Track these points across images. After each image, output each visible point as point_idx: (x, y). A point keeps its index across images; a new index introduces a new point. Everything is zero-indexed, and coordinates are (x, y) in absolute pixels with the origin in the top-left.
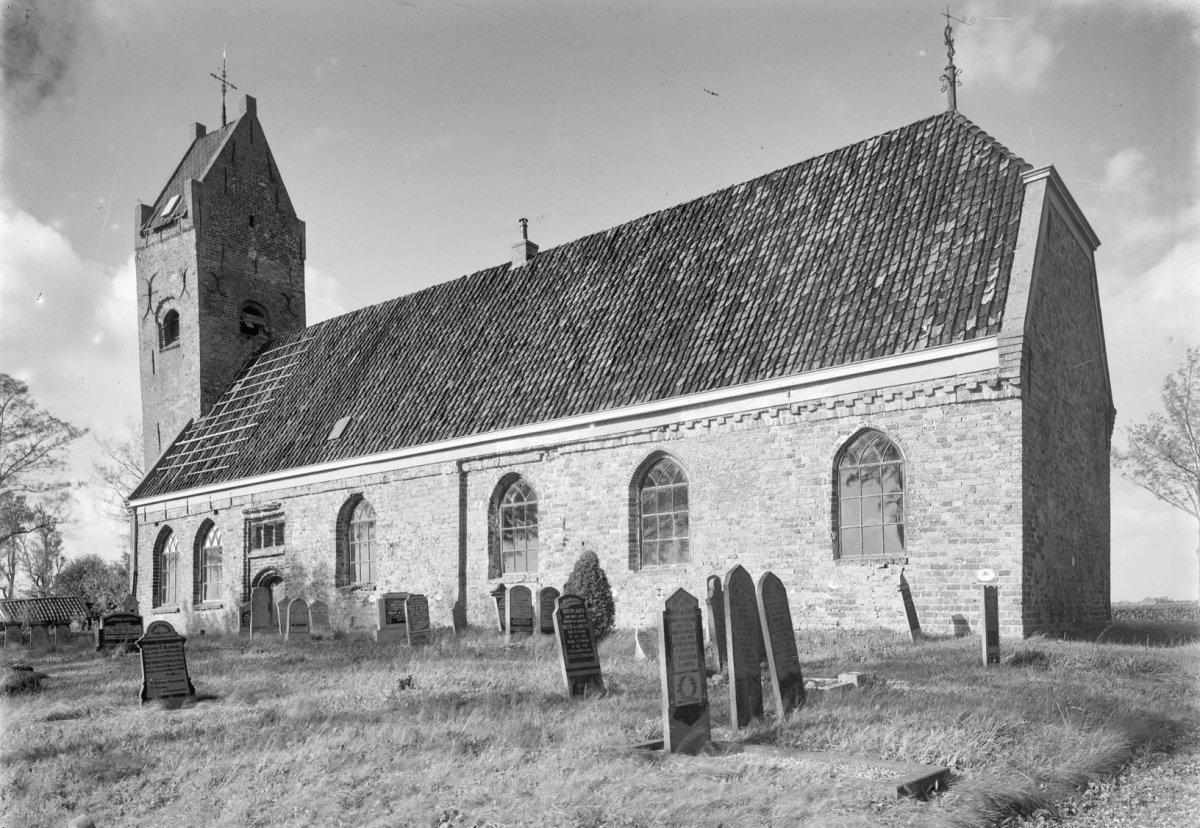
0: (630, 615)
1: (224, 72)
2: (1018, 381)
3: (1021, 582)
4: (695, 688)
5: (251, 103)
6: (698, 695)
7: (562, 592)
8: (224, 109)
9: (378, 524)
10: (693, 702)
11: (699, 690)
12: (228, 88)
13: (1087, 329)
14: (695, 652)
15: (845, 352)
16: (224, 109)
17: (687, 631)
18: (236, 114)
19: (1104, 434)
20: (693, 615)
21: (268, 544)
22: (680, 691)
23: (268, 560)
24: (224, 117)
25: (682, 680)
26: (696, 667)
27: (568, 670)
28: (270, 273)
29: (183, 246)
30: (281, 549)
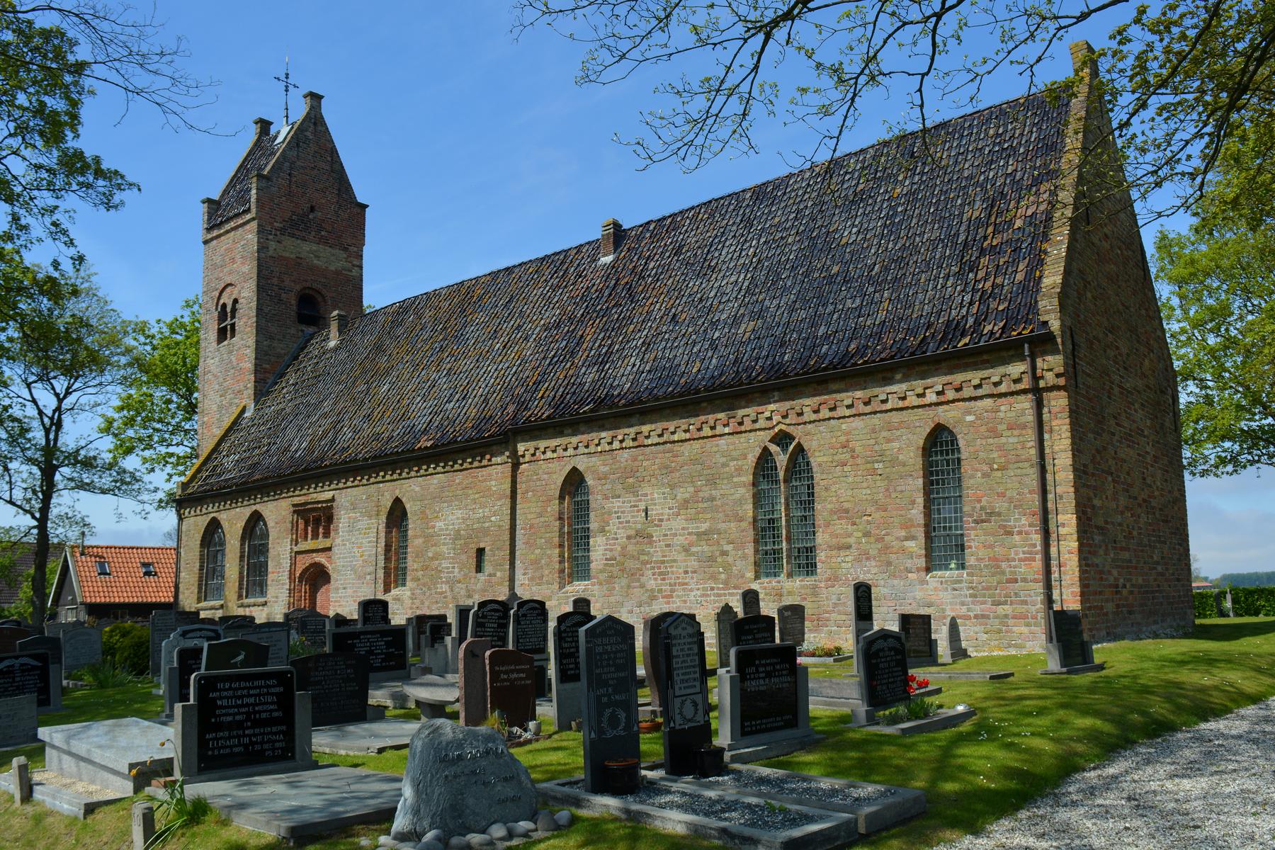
2: (660, 759)
3: (1077, 574)
4: (697, 710)
6: (700, 718)
11: (701, 712)
12: (291, 88)
13: (1143, 312)
14: (698, 675)
15: (1197, 41)
17: (688, 655)
18: (300, 111)
19: (753, 800)
22: (681, 713)
25: (683, 703)
26: (698, 690)
28: (326, 258)
29: (244, 240)
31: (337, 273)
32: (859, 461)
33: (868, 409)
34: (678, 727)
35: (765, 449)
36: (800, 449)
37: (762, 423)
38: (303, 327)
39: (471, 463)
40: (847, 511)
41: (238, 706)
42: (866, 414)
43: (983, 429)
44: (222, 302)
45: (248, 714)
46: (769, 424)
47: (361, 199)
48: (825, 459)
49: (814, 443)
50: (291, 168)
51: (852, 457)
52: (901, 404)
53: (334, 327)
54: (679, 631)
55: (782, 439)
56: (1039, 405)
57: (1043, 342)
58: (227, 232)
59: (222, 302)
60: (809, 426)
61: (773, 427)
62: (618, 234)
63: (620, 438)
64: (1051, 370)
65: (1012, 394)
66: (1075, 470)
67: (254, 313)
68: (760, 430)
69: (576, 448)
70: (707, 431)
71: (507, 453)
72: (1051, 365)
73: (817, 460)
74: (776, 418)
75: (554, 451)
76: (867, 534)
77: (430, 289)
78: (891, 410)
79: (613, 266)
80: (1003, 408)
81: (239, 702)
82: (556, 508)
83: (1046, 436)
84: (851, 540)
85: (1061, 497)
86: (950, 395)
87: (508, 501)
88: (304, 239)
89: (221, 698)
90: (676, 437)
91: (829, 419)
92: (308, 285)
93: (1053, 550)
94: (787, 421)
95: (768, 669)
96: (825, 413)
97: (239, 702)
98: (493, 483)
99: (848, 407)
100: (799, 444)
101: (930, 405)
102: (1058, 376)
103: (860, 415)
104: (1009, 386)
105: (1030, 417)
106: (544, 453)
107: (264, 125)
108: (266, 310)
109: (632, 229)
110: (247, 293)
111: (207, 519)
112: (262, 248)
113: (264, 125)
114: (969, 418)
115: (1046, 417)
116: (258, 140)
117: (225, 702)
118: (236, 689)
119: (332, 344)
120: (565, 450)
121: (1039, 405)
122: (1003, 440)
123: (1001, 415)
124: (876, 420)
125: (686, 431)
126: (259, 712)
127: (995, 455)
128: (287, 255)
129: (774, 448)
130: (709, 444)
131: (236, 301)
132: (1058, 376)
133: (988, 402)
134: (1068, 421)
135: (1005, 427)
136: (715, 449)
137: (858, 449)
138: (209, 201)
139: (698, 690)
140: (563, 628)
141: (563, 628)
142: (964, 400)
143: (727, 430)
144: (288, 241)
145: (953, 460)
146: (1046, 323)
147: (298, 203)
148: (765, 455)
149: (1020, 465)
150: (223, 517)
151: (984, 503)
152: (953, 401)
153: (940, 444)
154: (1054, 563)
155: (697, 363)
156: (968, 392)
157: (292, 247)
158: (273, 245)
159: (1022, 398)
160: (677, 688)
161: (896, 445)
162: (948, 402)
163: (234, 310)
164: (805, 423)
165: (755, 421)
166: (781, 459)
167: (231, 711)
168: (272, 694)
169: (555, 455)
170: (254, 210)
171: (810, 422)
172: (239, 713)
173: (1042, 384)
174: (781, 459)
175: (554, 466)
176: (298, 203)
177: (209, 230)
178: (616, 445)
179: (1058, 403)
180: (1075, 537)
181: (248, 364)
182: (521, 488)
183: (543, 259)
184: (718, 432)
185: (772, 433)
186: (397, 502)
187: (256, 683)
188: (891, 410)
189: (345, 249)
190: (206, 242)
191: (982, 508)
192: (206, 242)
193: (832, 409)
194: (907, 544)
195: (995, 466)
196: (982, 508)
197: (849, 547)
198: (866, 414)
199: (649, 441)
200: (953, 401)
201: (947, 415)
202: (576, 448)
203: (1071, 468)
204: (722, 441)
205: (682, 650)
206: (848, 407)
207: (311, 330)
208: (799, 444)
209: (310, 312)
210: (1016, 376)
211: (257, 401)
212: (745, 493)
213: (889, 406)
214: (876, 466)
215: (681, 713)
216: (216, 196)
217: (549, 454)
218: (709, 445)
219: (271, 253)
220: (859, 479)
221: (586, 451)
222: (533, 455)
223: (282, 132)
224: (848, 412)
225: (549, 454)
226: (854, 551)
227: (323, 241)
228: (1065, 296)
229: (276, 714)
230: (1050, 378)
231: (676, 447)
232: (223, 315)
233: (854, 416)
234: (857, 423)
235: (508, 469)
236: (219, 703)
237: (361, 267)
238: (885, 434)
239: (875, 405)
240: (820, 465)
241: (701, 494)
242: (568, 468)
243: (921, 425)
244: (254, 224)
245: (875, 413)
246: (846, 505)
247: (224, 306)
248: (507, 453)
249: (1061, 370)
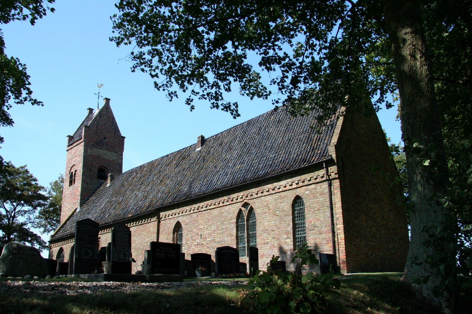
18: (102, 104)
26: (127, 250)
28: (109, 155)
29: (80, 149)
31: (113, 161)
32: (271, 211)
33: (274, 192)
34: (116, 261)
36: (252, 209)
37: (239, 200)
38: (100, 180)
39: (144, 222)
40: (267, 230)
42: (273, 194)
43: (312, 196)
44: (71, 171)
46: (242, 200)
47: (123, 135)
48: (260, 211)
49: (256, 206)
50: (97, 124)
51: (269, 210)
52: (285, 189)
53: (109, 179)
55: (246, 205)
56: (330, 185)
57: (330, 162)
58: (74, 146)
60: (255, 200)
61: (243, 201)
62: (203, 140)
63: (193, 209)
64: (333, 172)
65: (321, 182)
66: (342, 209)
67: (81, 174)
68: (238, 202)
69: (179, 214)
70: (221, 204)
71: (156, 217)
72: (333, 169)
73: (257, 211)
74: (244, 198)
75: (172, 216)
76: (273, 238)
77: (141, 164)
78: (281, 192)
79: (200, 151)
80: (318, 188)
82: (172, 236)
83: (333, 197)
84: (269, 241)
85: (338, 219)
86: (301, 184)
87: (156, 235)
88: (101, 149)
90: (211, 207)
91: (261, 197)
93: (336, 239)
94: (247, 198)
96: (260, 195)
98: (151, 228)
99: (267, 191)
101: (294, 189)
102: (336, 174)
103: (271, 194)
104: (320, 180)
105: (327, 190)
106: (168, 216)
107: (91, 110)
108: (86, 174)
109: (208, 138)
110: (79, 168)
111: (59, 248)
112: (85, 151)
113: (91, 110)
114: (307, 192)
115: (332, 190)
116: (88, 115)
119: (108, 185)
120: (175, 215)
121: (330, 185)
122: (318, 199)
123: (318, 190)
124: (276, 196)
125: (214, 205)
127: (316, 205)
128: (94, 154)
129: (243, 209)
131: (76, 171)
132: (336, 174)
133: (313, 186)
134: (339, 190)
135: (318, 194)
136: (224, 211)
137: (271, 207)
138: (69, 136)
139: (127, 250)
142: (305, 186)
143: (228, 203)
144: (95, 150)
145: (303, 208)
146: (331, 155)
148: (240, 211)
149: (324, 208)
150: (64, 247)
151: (313, 223)
152: (302, 187)
153: (297, 201)
154: (336, 244)
155: (220, 181)
156: (306, 183)
158: (89, 151)
159: (325, 183)
161: (283, 204)
162: (300, 187)
163: (75, 174)
164: (253, 199)
165: (237, 199)
169: (172, 217)
170: (83, 138)
171: (255, 198)
173: (331, 178)
174: (245, 213)
175: (172, 221)
177: (69, 146)
178: (192, 212)
179: (336, 184)
180: (343, 233)
181: (79, 193)
182: (161, 230)
183: (179, 151)
184: (225, 204)
185: (243, 203)
188: (281, 192)
189: (116, 153)
190: (68, 151)
191: (312, 225)
193: (262, 193)
194: (287, 240)
195: (316, 209)
196: (312, 225)
197: (267, 243)
198: (273, 194)
199: (202, 210)
200: (302, 187)
201: (299, 192)
202: (179, 214)
203: (341, 208)
204: (226, 208)
206: (267, 191)
207: (103, 181)
208: (251, 207)
209: (102, 176)
210: (322, 176)
211: (81, 206)
212: (234, 226)
213: (280, 190)
214: (277, 212)
216: (72, 135)
217: (170, 217)
218: (222, 209)
219: (88, 153)
220: (271, 218)
221: (182, 214)
222: (165, 217)
223: (96, 112)
224: (267, 194)
225: (170, 217)
226: (269, 245)
227: (108, 149)
228: (338, 147)
230: (333, 176)
231: (211, 211)
232: (71, 177)
233: (269, 195)
234: (270, 197)
235: (156, 223)
237: (122, 159)
238: (279, 200)
239: (276, 190)
240: (258, 214)
241: (219, 228)
242: (176, 221)
243: (291, 196)
244: (83, 143)
245: (276, 193)
246: (267, 228)
247: (72, 173)
248: (156, 217)
249: (336, 172)
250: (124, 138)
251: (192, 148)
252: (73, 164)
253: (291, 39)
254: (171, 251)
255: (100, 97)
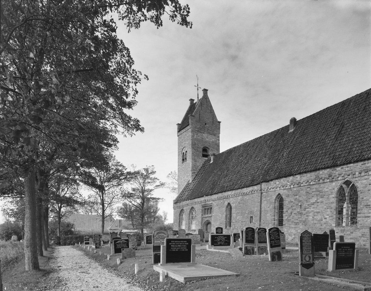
0: (198, 216)
1: (198, 84)
5: (205, 91)
7: (157, 215)
8: (198, 95)
9: (201, 150)
10: (309, 263)
14: (310, 249)
16: (198, 95)
18: (201, 95)
20: (310, 238)
21: (207, 214)
23: (207, 218)
24: (198, 97)
25: (306, 256)
26: (311, 253)
27: (267, 245)
30: (210, 215)
31: (213, 142)
34: (303, 263)
35: (341, 186)
41: (177, 247)
44: (183, 152)
45: (179, 249)
47: (219, 120)
54: (305, 235)
59: (183, 152)
81: (177, 246)
89: (172, 245)
92: (205, 146)
95: (346, 250)
97: (177, 246)
100: (353, 185)
112: (193, 136)
117: (173, 246)
118: (176, 243)
126: (182, 249)
130: (322, 185)
131: (186, 152)
140: (270, 232)
141: (270, 232)
143: (328, 180)
144: (199, 134)
147: (199, 118)
148: (341, 188)
157: (199, 136)
160: (304, 251)
166: (347, 190)
167: (175, 248)
168: (185, 245)
172: (177, 249)
174: (347, 190)
176: (199, 118)
185: (344, 181)
186: (229, 204)
187: (178, 242)
192: (178, 136)
205: (306, 241)
208: (353, 185)
215: (305, 259)
216: (180, 123)
229: (186, 250)
236: (172, 246)
237: (219, 140)
247: (184, 153)
250: (220, 122)
251: (286, 128)
252: (184, 146)
253: (123, 108)
254: (349, 249)
255: (199, 88)
